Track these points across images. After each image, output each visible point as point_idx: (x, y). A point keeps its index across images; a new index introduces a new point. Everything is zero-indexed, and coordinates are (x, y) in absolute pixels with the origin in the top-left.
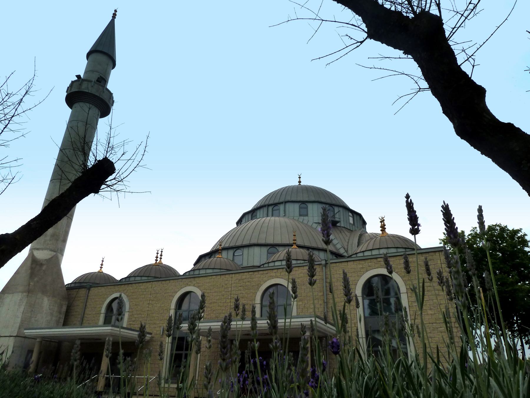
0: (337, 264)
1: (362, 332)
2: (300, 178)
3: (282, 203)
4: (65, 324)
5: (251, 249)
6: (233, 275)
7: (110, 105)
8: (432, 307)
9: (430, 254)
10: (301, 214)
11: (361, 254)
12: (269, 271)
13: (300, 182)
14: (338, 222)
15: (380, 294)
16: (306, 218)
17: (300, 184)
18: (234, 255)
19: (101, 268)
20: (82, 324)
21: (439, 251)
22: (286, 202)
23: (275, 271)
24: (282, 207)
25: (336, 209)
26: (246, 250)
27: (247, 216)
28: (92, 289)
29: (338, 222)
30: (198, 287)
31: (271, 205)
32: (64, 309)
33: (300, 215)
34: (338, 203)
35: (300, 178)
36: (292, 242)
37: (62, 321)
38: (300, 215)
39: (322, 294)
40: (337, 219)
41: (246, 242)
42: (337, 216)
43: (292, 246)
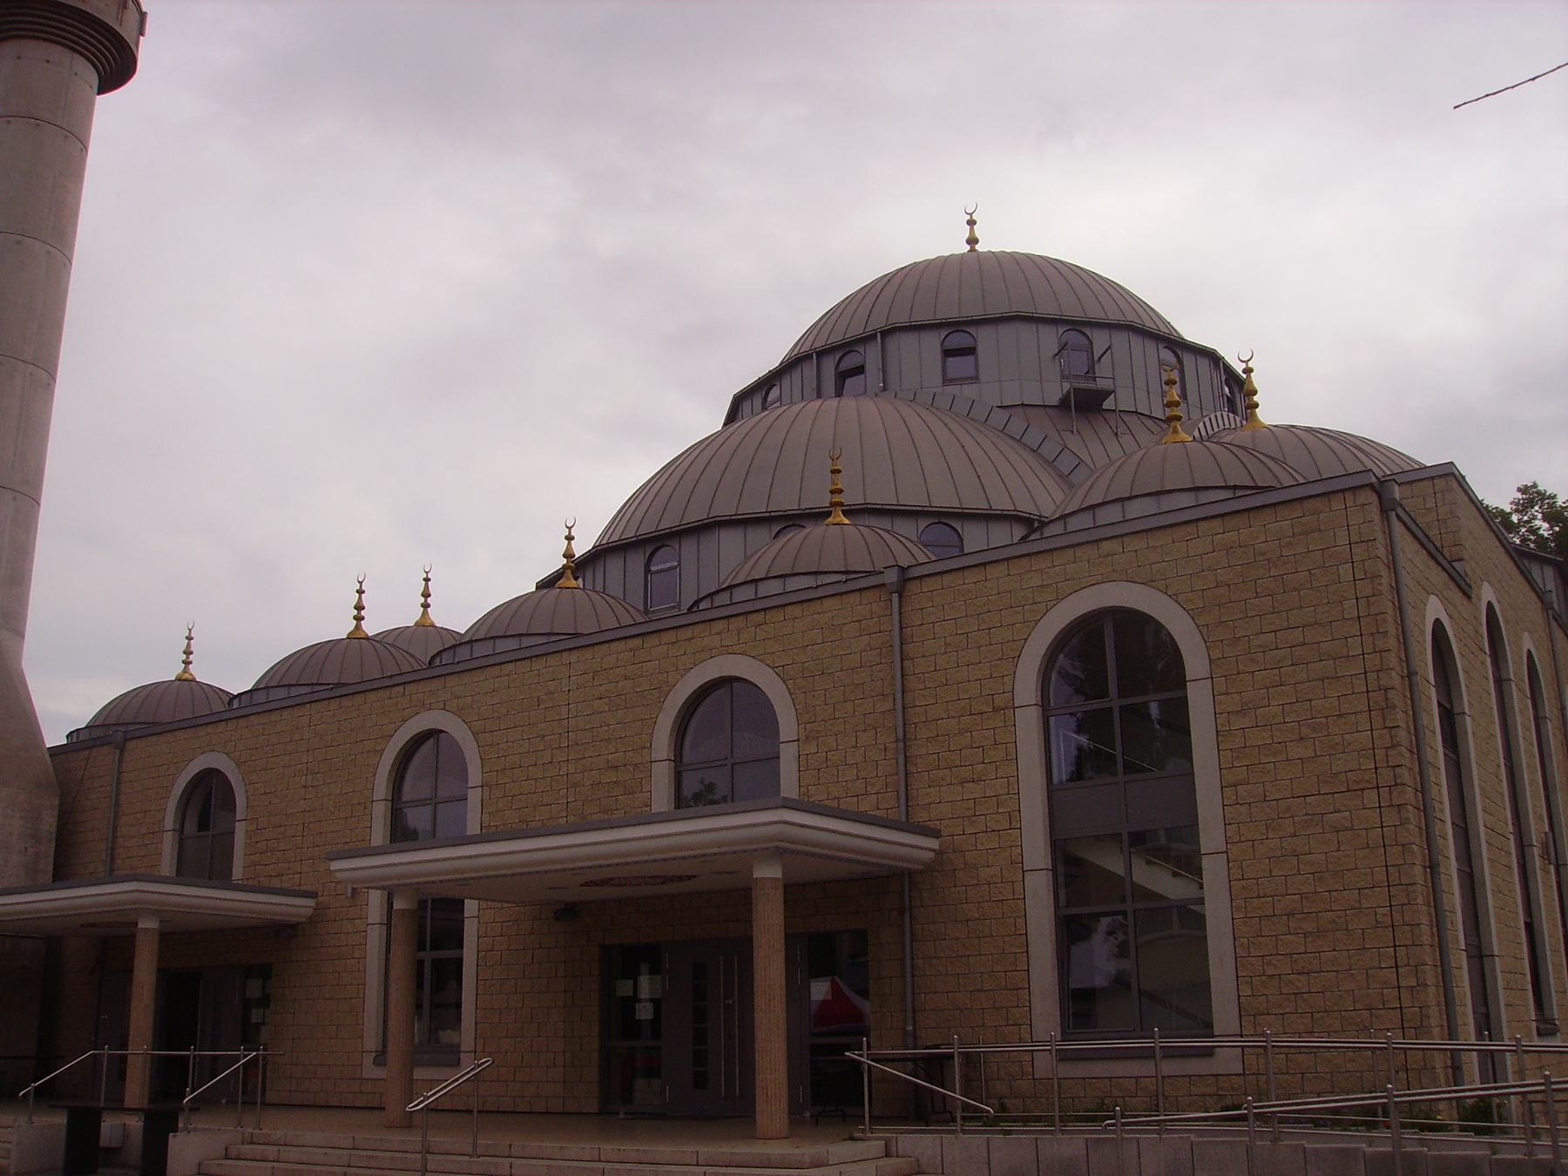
0: (947, 579)
1: (1035, 847)
2: (971, 223)
3: (872, 337)
4: (62, 874)
5: (708, 542)
6: (574, 656)
7: (126, 32)
8: (1305, 731)
9: (1309, 505)
10: (949, 376)
11: (1084, 521)
12: (697, 629)
13: (972, 241)
14: (1106, 394)
15: (1118, 688)
16: (970, 391)
17: (972, 250)
18: (647, 570)
19: (187, 663)
20: (112, 871)
21: (1343, 491)
22: (886, 333)
23: (720, 625)
24: (871, 355)
25: (1100, 340)
26: (688, 546)
27: (746, 406)
28: (131, 745)
29: (1106, 394)
30: (459, 712)
31: (832, 349)
32: (49, 822)
33: (947, 381)
34: (1114, 316)
35: (971, 223)
36: (824, 501)
37: (48, 864)
38: (947, 381)
39: (888, 705)
40: (1102, 384)
41: (696, 515)
42: (1103, 369)
43: (829, 514)
